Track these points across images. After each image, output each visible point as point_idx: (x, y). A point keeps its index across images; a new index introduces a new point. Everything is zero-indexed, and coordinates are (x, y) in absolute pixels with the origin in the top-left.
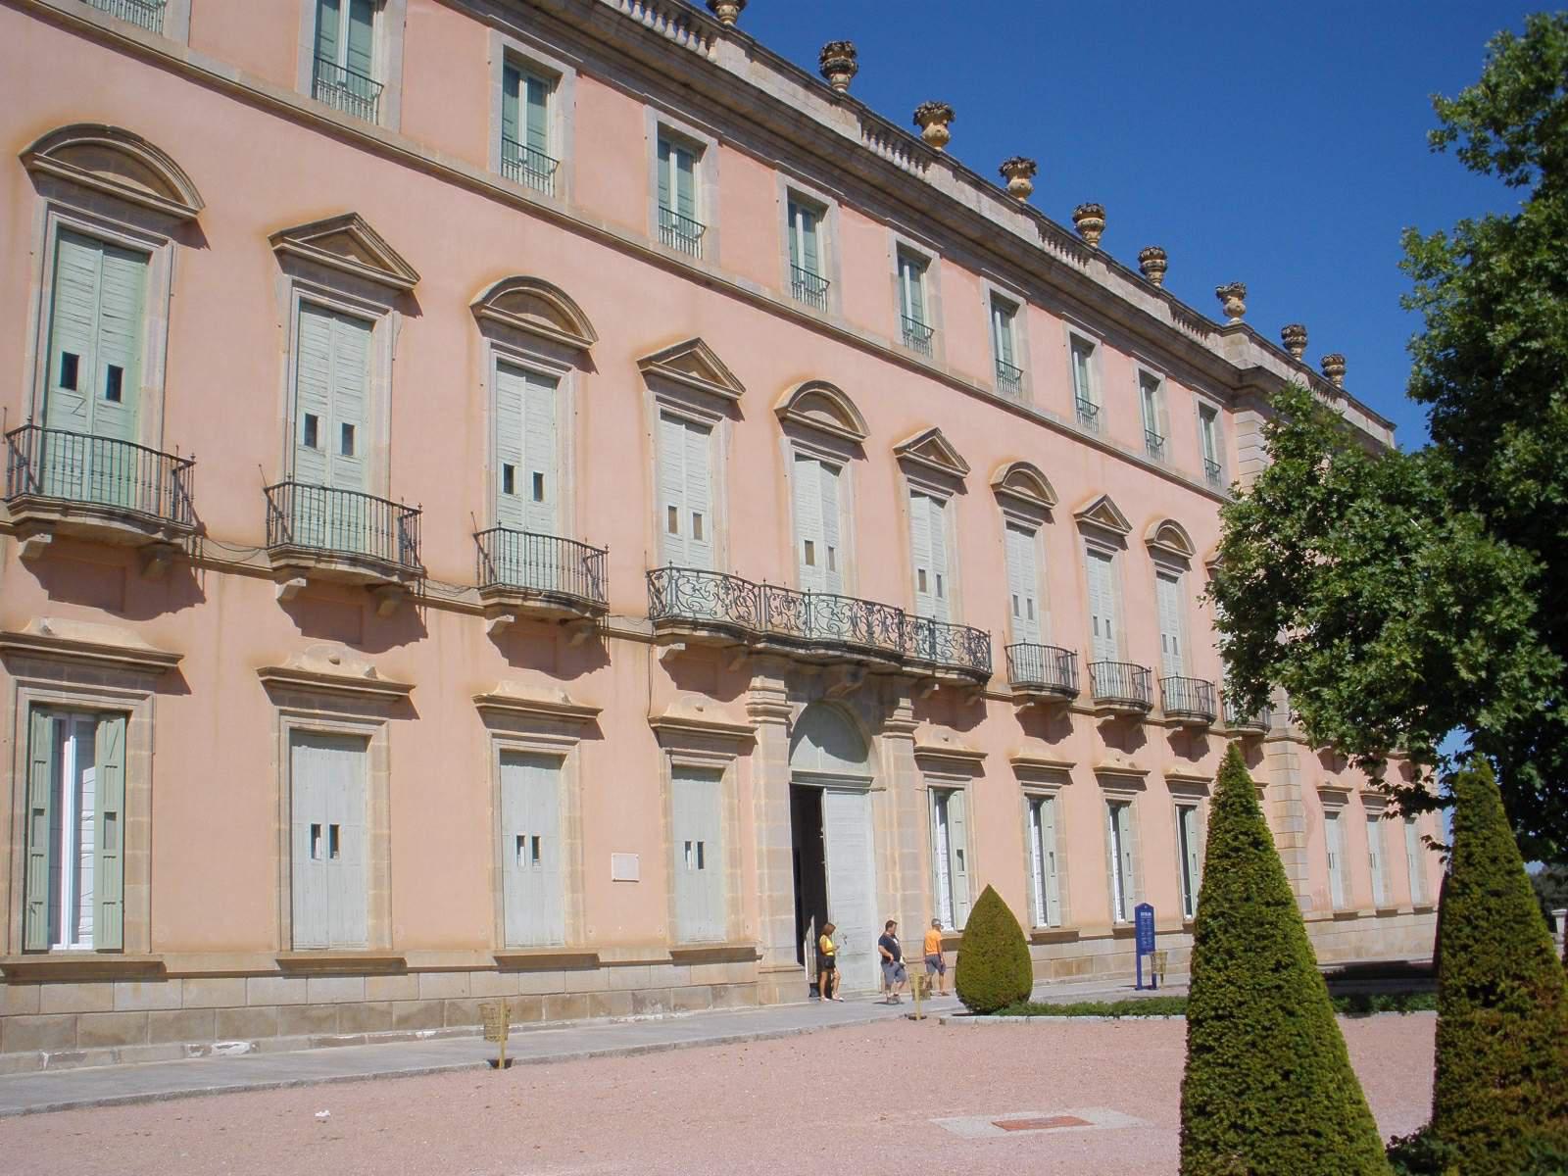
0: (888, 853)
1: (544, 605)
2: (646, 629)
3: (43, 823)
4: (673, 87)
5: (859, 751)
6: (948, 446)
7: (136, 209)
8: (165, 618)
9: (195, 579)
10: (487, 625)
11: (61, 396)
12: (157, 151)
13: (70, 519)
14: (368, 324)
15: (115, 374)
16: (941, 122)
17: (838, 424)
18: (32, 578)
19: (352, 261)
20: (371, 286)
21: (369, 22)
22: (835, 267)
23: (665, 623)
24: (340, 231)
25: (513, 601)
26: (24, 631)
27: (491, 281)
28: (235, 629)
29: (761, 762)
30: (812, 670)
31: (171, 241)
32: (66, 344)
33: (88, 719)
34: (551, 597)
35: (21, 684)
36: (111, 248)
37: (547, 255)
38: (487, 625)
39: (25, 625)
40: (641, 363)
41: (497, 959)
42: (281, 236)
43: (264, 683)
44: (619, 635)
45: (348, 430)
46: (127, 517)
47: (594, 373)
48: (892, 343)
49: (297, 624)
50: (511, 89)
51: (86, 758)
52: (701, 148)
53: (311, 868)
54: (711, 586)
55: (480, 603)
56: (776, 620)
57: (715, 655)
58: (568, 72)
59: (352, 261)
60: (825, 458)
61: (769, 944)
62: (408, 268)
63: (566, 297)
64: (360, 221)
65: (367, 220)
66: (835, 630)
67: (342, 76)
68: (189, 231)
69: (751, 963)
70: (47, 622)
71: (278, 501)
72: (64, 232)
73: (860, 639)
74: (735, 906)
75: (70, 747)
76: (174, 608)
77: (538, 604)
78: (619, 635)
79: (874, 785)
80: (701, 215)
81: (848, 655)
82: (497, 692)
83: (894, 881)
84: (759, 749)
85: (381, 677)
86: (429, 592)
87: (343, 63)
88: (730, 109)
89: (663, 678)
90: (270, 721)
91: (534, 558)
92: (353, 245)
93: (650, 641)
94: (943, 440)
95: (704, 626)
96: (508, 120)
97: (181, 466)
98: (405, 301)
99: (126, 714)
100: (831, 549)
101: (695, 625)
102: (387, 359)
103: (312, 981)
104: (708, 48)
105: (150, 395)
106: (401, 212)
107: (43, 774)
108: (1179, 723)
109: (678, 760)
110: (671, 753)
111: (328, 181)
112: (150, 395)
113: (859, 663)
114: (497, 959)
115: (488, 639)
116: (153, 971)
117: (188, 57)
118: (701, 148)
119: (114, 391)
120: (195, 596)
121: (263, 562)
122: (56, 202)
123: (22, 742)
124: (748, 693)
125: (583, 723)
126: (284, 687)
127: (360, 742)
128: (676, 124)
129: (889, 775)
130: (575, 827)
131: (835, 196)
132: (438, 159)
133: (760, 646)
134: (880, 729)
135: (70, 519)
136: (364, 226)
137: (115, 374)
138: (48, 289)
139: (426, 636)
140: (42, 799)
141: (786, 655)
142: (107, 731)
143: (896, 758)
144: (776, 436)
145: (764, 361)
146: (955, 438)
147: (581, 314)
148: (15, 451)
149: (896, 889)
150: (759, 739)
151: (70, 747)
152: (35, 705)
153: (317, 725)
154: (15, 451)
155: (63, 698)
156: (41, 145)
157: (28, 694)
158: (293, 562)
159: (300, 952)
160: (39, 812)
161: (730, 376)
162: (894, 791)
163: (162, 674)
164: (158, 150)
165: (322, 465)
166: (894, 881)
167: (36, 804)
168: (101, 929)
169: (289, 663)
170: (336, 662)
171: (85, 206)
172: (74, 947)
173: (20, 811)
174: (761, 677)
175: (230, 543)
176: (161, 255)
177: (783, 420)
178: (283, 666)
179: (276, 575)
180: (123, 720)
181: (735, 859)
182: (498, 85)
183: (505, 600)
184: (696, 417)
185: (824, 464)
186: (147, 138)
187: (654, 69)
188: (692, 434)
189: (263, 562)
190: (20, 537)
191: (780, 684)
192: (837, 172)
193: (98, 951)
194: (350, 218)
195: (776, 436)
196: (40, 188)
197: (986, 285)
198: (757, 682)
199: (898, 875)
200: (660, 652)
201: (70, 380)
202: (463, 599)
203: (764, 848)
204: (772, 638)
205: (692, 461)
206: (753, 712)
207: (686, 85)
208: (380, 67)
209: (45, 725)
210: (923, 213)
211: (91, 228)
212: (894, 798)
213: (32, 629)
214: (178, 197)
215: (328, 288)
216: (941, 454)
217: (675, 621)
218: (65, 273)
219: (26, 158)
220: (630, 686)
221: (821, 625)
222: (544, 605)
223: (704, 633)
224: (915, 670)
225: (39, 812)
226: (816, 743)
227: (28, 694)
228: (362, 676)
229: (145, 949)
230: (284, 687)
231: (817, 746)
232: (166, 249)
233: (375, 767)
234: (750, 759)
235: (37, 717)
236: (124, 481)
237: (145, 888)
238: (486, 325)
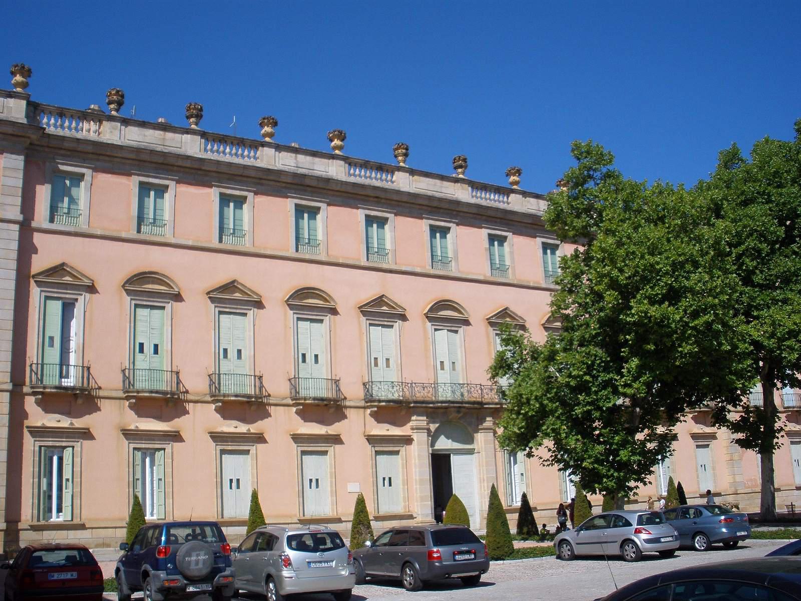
0: (482, 476)
1: (313, 402)
2: (121, 394)
3: (139, 483)
4: (372, 199)
5: (471, 440)
6: (514, 313)
7: (66, 286)
8: (176, 420)
9: (97, 403)
10: (294, 409)
11: (139, 356)
12: (163, 275)
13: (140, 394)
14: (245, 315)
15: (156, 346)
16: (515, 176)
17: (322, 302)
18: (133, 413)
19: (237, 295)
20: (300, 307)
21: (503, 246)
22: (456, 252)
23: (369, 399)
24: (231, 286)
25: (301, 401)
26: (130, 428)
27: (547, 315)
28: (201, 420)
29: (416, 447)
30: (442, 410)
31: (171, 302)
32: (139, 340)
33: (61, 449)
34: (314, 399)
35: (298, 446)
36: (153, 307)
37: (313, 276)
38: (294, 409)
39: (130, 426)
40: (359, 308)
41: (299, 520)
42: (208, 293)
43: (210, 436)
44: (350, 407)
45: (239, 351)
46: (157, 392)
47: (339, 316)
48: (485, 276)
49: (136, 414)
50: (545, 253)
51: (152, 464)
52: (505, 238)
53: (309, 493)
54: (386, 387)
55: (210, 399)
56: (486, 396)
57: (394, 411)
58: (323, 206)
59: (237, 295)
60: (449, 328)
61: (420, 513)
62: (523, 319)
63: (323, 291)
64: (238, 282)
65: (240, 281)
66: (445, 396)
67: (498, 266)
68: (334, 311)
69: (411, 520)
70: (137, 424)
71: (294, 382)
72: (298, 319)
73: (458, 397)
74: (407, 499)
75: (148, 460)
76: (262, 419)
77: (310, 402)
78: (350, 407)
79: (475, 451)
80: (388, 245)
81: (452, 405)
82: (299, 432)
83: (484, 487)
84: (415, 443)
85: (252, 431)
86: (270, 401)
87: (498, 263)
88: (399, 201)
89: (371, 421)
90: (295, 449)
91: (238, 383)
92: (236, 289)
93: (365, 408)
94: (511, 311)
95: (383, 401)
96: (545, 263)
97: (337, 382)
98: (259, 305)
99: (164, 449)
100: (453, 363)
101: (380, 401)
102: (398, 336)
103: (228, 528)
104: (508, 199)
105: (167, 351)
106: (400, 291)
107: (139, 469)
108: (218, 401)
109: (377, 449)
110: (374, 447)
111: (370, 286)
112: (167, 351)
113: (460, 407)
114: (299, 520)
115: (215, 412)
116: (82, 527)
117: (173, 241)
118: (505, 238)
119: (156, 351)
120: (268, 415)
121: (209, 398)
122: (133, 298)
123: (131, 460)
124: (411, 422)
125: (336, 440)
126: (217, 437)
127: (247, 452)
128: (373, 213)
129: (482, 447)
130: (334, 475)
131: (454, 223)
132: (269, 252)
133: (412, 405)
134: (477, 431)
135: (140, 394)
136: (239, 283)
137: (156, 346)
138: (132, 325)
139: (271, 416)
140: (139, 475)
141: (426, 407)
142: (158, 455)
143: (485, 440)
144: (424, 324)
145: (414, 296)
146: (517, 309)
147: (329, 296)
148: (211, 380)
149: (485, 491)
150: (415, 439)
151: (148, 460)
152: (135, 449)
153: (230, 448)
154: (211, 380)
155: (143, 446)
156: (126, 283)
157: (132, 446)
158: (216, 398)
159: (308, 516)
160: (138, 479)
161: (520, 317)
162: (484, 453)
163: (86, 434)
164: (164, 275)
165: (305, 371)
166: (484, 487)
167: (136, 477)
168: (159, 514)
169: (219, 430)
170: (236, 427)
171: (67, 289)
172: (152, 518)
173: (131, 479)
174: (415, 416)
175: (197, 394)
176: (461, 330)
177: (427, 317)
178: (215, 431)
179: (213, 402)
180: (163, 451)
181: (406, 482)
182: (541, 251)
183: (298, 401)
184: (386, 323)
185: (448, 330)
186: (160, 272)
187: (361, 195)
188: (384, 329)
189: (209, 398)
190: (128, 400)
191: (425, 418)
192: (455, 213)
193: (158, 519)
194: (234, 281)
195: (424, 324)
196: (291, 309)
197: (539, 241)
198: (414, 418)
199: (486, 485)
200: (368, 411)
201: (141, 350)
202: (284, 402)
203: (418, 478)
204: (415, 402)
205: (385, 340)
206: (412, 429)
207: (376, 197)
208: (246, 226)
209: (139, 454)
210: (501, 219)
211: (145, 303)
212: (484, 456)
213: (132, 427)
214: (172, 288)
215: (228, 306)
216: (510, 316)
217: (374, 401)
218: (138, 318)
219: (123, 286)
220: (356, 426)
221: (445, 394)
222: (313, 402)
223: (384, 404)
224: (491, 406)
225: (138, 479)
226: (448, 438)
227: (132, 446)
228: (245, 431)
229: (171, 518)
230: (217, 437)
231: (448, 439)
232: (170, 304)
233: (402, 460)
234: (412, 446)
235: (136, 452)
236: (161, 382)
237: (171, 500)
238: (291, 307)
